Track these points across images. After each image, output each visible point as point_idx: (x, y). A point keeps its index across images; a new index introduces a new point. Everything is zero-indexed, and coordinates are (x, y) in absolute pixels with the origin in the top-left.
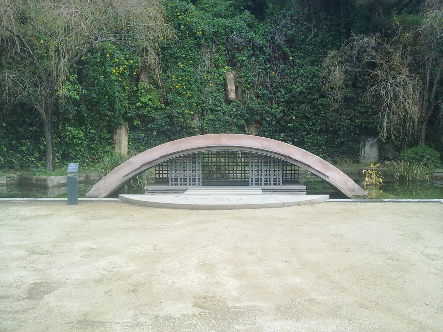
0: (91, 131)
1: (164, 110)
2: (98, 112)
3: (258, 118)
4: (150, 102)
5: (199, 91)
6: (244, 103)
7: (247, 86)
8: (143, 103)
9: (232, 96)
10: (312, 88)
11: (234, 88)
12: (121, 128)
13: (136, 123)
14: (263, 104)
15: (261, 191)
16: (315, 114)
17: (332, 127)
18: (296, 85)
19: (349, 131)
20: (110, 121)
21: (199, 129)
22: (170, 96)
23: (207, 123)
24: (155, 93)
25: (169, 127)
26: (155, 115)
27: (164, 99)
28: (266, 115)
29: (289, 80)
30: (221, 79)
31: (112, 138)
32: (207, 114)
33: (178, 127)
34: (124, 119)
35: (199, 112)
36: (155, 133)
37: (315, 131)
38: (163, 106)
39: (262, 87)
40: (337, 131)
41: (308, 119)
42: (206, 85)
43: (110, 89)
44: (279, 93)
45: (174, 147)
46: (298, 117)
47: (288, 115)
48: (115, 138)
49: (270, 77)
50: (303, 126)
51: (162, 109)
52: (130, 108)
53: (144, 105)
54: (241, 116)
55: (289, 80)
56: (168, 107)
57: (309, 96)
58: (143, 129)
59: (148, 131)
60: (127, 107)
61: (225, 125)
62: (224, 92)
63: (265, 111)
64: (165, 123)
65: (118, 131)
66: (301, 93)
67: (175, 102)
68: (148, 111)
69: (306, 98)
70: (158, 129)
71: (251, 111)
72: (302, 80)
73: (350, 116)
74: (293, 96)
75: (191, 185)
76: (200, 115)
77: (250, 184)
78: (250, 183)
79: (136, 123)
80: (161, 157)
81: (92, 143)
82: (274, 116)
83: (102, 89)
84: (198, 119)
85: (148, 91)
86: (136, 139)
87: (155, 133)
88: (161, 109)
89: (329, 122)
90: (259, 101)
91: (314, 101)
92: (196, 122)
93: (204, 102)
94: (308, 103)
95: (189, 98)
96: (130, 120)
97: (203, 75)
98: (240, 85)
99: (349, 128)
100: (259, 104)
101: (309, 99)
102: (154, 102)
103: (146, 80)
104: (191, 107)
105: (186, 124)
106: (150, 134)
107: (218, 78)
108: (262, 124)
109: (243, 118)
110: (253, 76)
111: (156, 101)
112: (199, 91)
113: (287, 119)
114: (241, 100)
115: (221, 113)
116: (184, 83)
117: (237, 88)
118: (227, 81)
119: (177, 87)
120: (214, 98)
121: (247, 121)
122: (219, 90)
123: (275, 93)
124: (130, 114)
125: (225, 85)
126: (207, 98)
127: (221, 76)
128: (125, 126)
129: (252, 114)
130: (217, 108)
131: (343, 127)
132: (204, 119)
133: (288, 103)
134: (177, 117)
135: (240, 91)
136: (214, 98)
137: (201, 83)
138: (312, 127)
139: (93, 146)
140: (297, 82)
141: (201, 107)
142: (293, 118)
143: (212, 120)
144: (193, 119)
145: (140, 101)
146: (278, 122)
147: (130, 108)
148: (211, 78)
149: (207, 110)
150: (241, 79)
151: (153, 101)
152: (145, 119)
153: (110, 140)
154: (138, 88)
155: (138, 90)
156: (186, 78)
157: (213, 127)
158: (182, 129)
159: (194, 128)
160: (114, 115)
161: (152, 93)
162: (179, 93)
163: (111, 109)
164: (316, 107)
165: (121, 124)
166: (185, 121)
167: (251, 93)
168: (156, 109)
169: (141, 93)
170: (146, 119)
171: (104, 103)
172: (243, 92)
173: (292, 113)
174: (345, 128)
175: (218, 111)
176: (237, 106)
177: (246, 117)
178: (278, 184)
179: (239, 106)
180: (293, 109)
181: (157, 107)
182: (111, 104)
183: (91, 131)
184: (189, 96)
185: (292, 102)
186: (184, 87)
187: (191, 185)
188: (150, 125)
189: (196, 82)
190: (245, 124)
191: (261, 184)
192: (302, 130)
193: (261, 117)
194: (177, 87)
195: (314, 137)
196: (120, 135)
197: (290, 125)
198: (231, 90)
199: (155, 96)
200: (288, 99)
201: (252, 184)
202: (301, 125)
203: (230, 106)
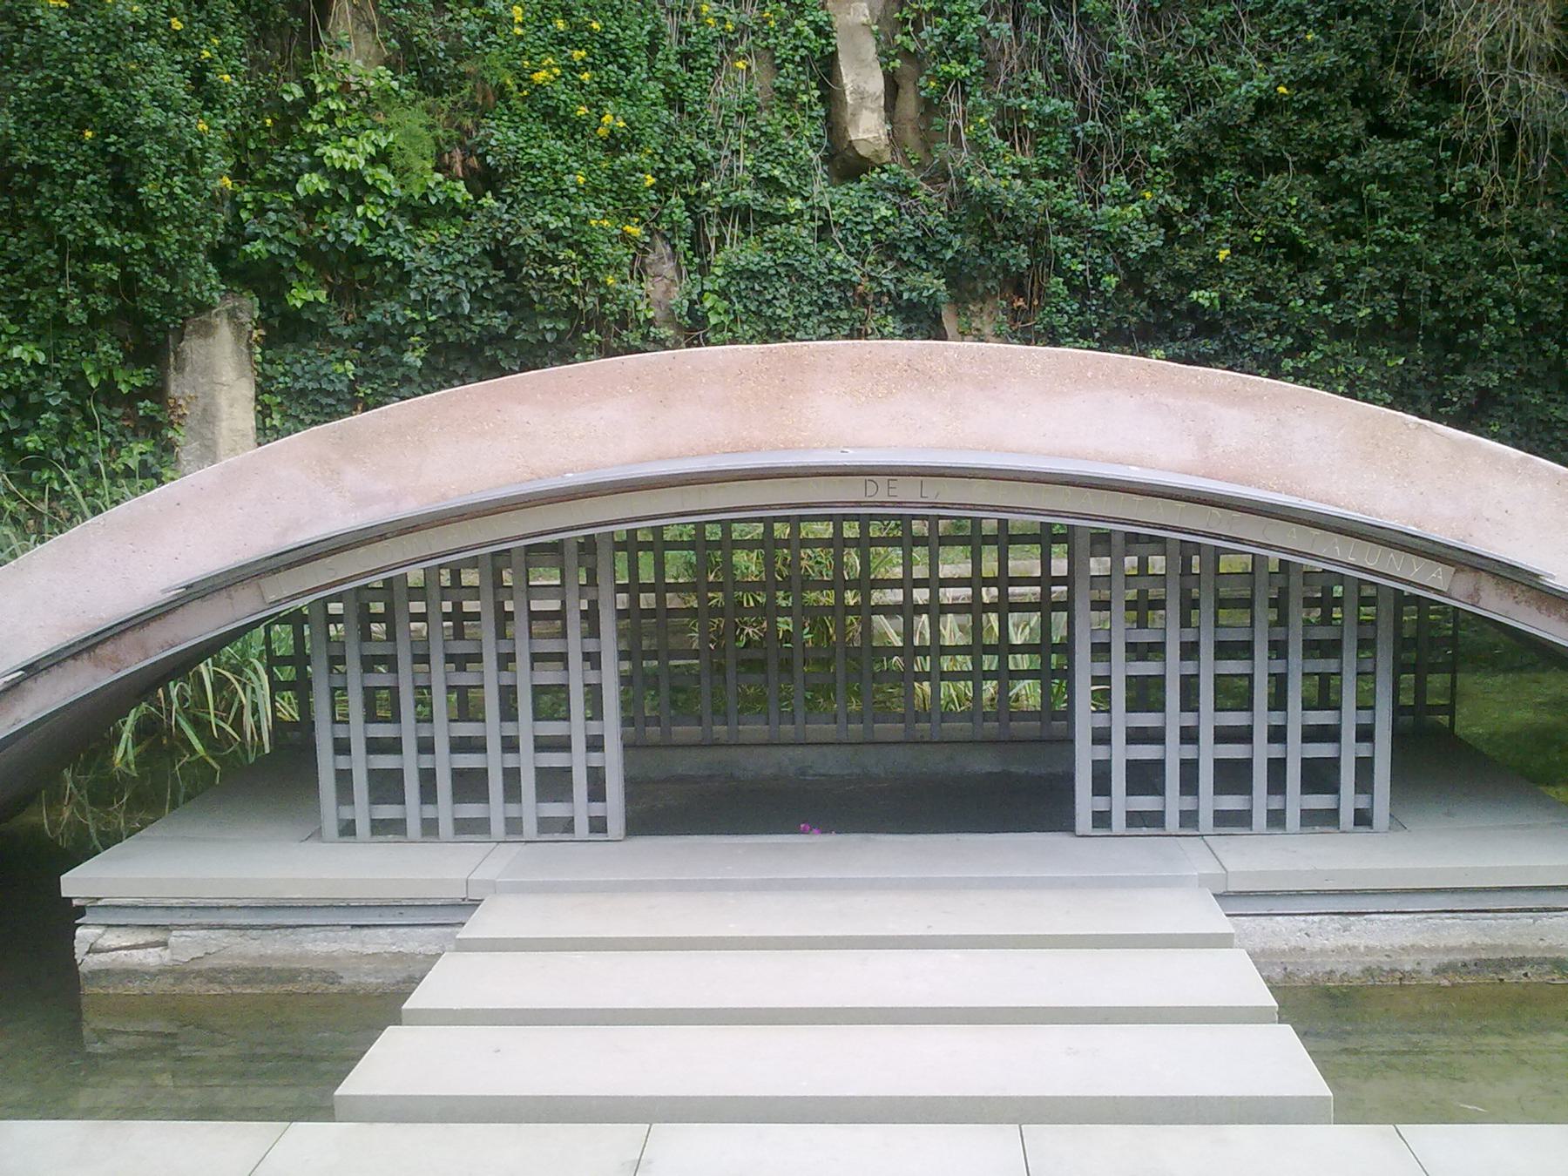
0: (16, 352)
1: (467, 217)
2: (51, 237)
3: (1020, 256)
4: (383, 173)
5: (675, 101)
6: (939, 175)
7: (955, 68)
8: (340, 175)
9: (868, 129)
10: (1326, 80)
11: (876, 84)
12: (207, 330)
13: (298, 297)
14: (1045, 174)
15: (1283, 1061)
16: (1345, 231)
17: (1434, 304)
18: (1231, 65)
19: (1528, 325)
20: (129, 284)
21: (679, 327)
22: (500, 135)
23: (723, 294)
24: (415, 119)
25: (498, 321)
26: (415, 250)
27: (469, 152)
28: (1063, 242)
29: (1193, 35)
30: (798, 34)
31: (157, 392)
32: (721, 239)
33: (552, 315)
34: (224, 275)
35: (675, 227)
36: (413, 358)
37: (1341, 331)
38: (461, 193)
39: (1037, 77)
40: (1463, 325)
41: (1300, 257)
42: (717, 69)
43: (108, 81)
44: (1133, 113)
45: (353, 477)
46: (1244, 251)
47: (1192, 240)
48: (173, 389)
49: (1085, 17)
50: (1270, 299)
51: (457, 211)
52: (260, 211)
53: (343, 191)
54: (920, 249)
55: (1193, 35)
56: (488, 200)
57: (1312, 127)
58: (346, 333)
59: (379, 345)
60: (243, 205)
61: (828, 305)
62: (819, 110)
63: (1059, 216)
64: (475, 297)
65: (193, 347)
66: (1265, 106)
67: (531, 166)
68: (368, 221)
69: (1288, 136)
70: (432, 332)
71: (982, 215)
72: (1266, 37)
73: (1540, 240)
74: (1224, 130)
75: (530, 827)
76: (683, 245)
77: (1083, 819)
78: (1085, 802)
79: (298, 297)
80: (197, 593)
81: (28, 423)
82: (1115, 244)
83: (58, 86)
84: (668, 268)
85: (370, 106)
86: (303, 392)
87: (413, 358)
88: (450, 210)
89: (1421, 280)
90: (1026, 161)
91: (1334, 156)
92: (662, 286)
93: (704, 169)
94: (1303, 167)
95: (613, 145)
96: (264, 281)
97: (697, 13)
98: (910, 69)
99: (1534, 312)
100: (1023, 174)
101: (1310, 140)
102: (407, 170)
103: (366, 44)
104: (626, 202)
105: (603, 300)
106: (387, 364)
107: (784, 24)
108: (1042, 293)
109: (930, 257)
110: (982, 12)
111: (417, 164)
112: (675, 101)
113: (1186, 262)
114: (916, 155)
115: (803, 233)
116: (578, 55)
117: (893, 86)
118: (839, 41)
119: (540, 77)
120: (762, 140)
121: (955, 275)
122: (791, 96)
123: (1109, 115)
124: (259, 244)
125: (825, 68)
126: (719, 146)
127: (800, 15)
128: (232, 315)
129: (986, 233)
130: (777, 203)
131: (1499, 302)
132: (704, 270)
133: (1189, 168)
134: (543, 259)
135: (909, 105)
136: (762, 140)
137: (684, 58)
138: (1327, 309)
139: (32, 442)
140: (1234, 47)
141: (686, 196)
142: (1223, 254)
143: (753, 276)
144: (640, 274)
145: (317, 165)
146: (1133, 279)
147: (260, 211)
148: (742, 29)
149: (724, 215)
150: (918, 27)
151: (398, 162)
152: (355, 275)
153: (145, 406)
154: (308, 87)
155: (312, 97)
156: (595, 25)
157: (758, 314)
158: (577, 331)
159: (650, 322)
160: (150, 250)
161: (394, 119)
162: (554, 116)
163: (127, 210)
164: (1350, 190)
165: (203, 307)
166: (595, 282)
167: (977, 110)
168: (418, 213)
169: (330, 117)
170: (362, 273)
171: (74, 175)
172: (930, 107)
173: (1208, 226)
174: (1511, 310)
175: (787, 219)
176: (894, 189)
177: (949, 254)
178: (1347, 816)
179: (906, 192)
180: (1216, 206)
181: (425, 197)
182: (122, 178)
183: (16, 352)
184: (612, 134)
185: (1211, 163)
186: (585, 77)
187: (530, 827)
188: (386, 311)
189: (652, 49)
190: (943, 295)
191: (1189, 819)
192: (1271, 325)
193: (1034, 252)
194: (540, 77)
195: (1337, 364)
196: (208, 370)
197: (1201, 296)
198: (861, 95)
199: (409, 134)
200: (1188, 145)
201: (1102, 819)
202: (1262, 295)
203: (853, 194)
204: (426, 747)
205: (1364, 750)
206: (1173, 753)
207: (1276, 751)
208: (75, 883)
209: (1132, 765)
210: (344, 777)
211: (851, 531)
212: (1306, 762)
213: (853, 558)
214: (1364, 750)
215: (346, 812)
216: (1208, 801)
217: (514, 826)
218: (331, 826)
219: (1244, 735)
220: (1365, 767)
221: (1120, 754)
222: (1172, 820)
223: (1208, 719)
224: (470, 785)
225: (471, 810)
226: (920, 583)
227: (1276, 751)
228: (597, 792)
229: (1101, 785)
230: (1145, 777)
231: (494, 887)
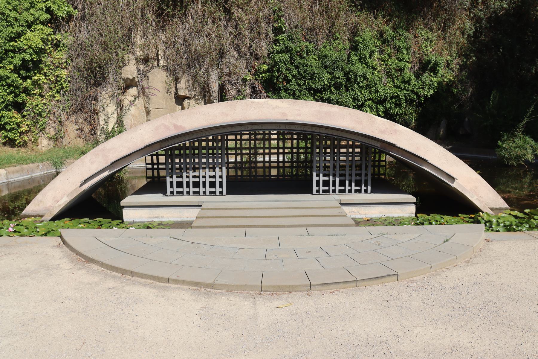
77: (314, 192)
78: (315, 188)
187: (208, 193)
201: (172, 193)
204: (188, 177)
207: (187, 180)
208: (123, 203)
209: (177, 182)
213: (281, 145)
219: (360, 175)
222: (185, 193)
227: (187, 180)
228: (221, 186)
229: (318, 184)
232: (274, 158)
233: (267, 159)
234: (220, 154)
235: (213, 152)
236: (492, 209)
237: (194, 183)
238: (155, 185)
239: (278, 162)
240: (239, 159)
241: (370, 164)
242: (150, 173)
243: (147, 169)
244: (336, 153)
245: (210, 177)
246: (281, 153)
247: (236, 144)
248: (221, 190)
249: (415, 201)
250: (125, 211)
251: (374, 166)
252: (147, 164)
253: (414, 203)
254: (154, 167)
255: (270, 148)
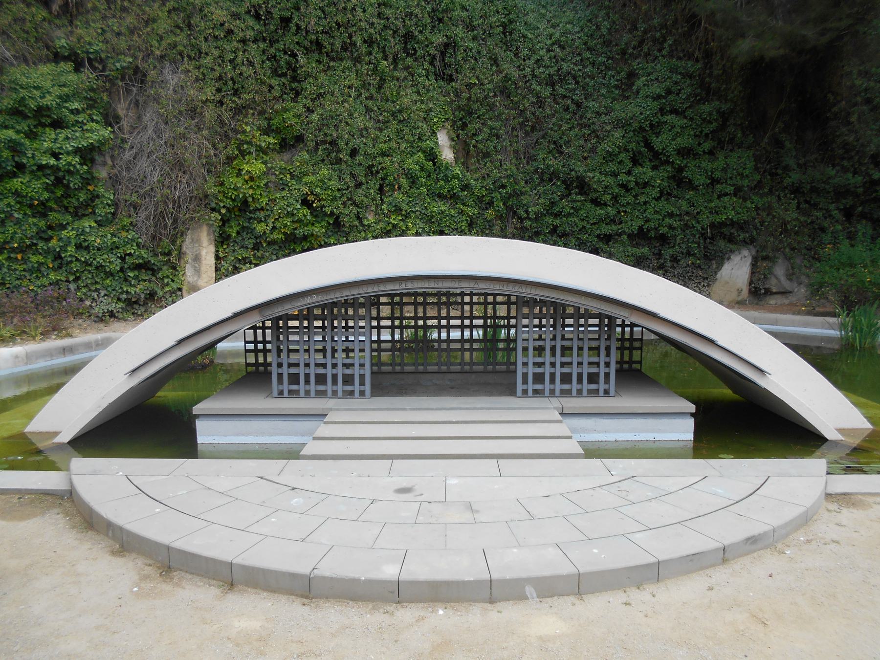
78: (520, 387)
201: (525, 392)
204: (553, 365)
205: (607, 370)
206: (575, 370)
208: (197, 409)
210: (280, 376)
211: (490, 299)
212: (534, 374)
214: (607, 370)
215: (281, 387)
216: (558, 386)
217: (335, 393)
218: (275, 393)
220: (607, 375)
221: (531, 370)
223: (559, 359)
224: (566, 378)
225: (321, 388)
226: (421, 318)
227: (552, 370)
230: (539, 378)
231: (331, 409)
232: (455, 334)
233: (444, 335)
234: (305, 328)
235: (541, 322)
236: (840, 431)
237: (563, 375)
238: (255, 376)
239: (393, 341)
240: (467, 333)
241: (614, 345)
242: (251, 359)
243: (247, 351)
244: (281, 328)
245: (317, 365)
246: (397, 327)
247: (425, 312)
248: (606, 387)
249: (694, 411)
250: (200, 425)
251: (621, 349)
252: (246, 342)
253: (692, 415)
254: (258, 348)
255: (379, 318)
